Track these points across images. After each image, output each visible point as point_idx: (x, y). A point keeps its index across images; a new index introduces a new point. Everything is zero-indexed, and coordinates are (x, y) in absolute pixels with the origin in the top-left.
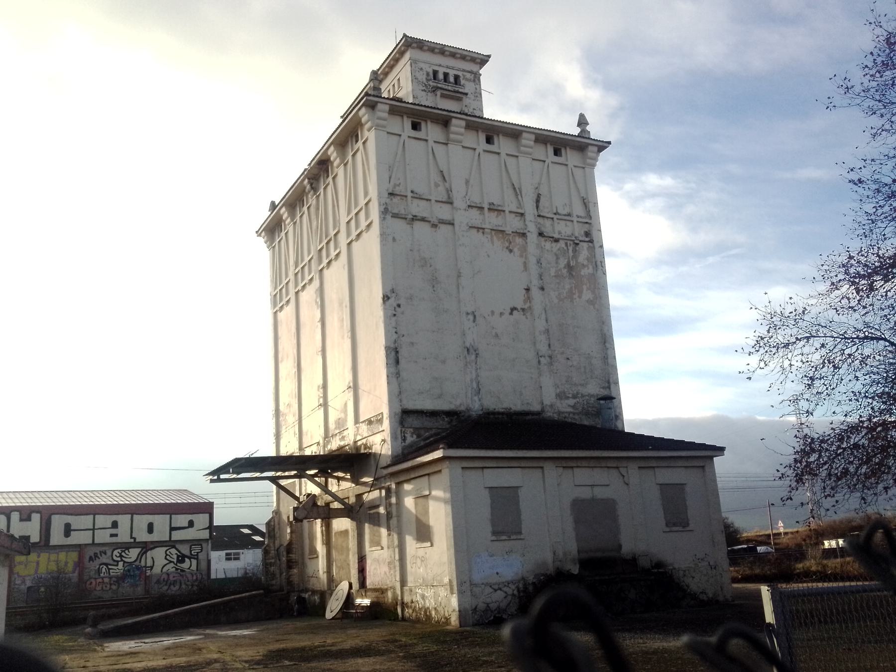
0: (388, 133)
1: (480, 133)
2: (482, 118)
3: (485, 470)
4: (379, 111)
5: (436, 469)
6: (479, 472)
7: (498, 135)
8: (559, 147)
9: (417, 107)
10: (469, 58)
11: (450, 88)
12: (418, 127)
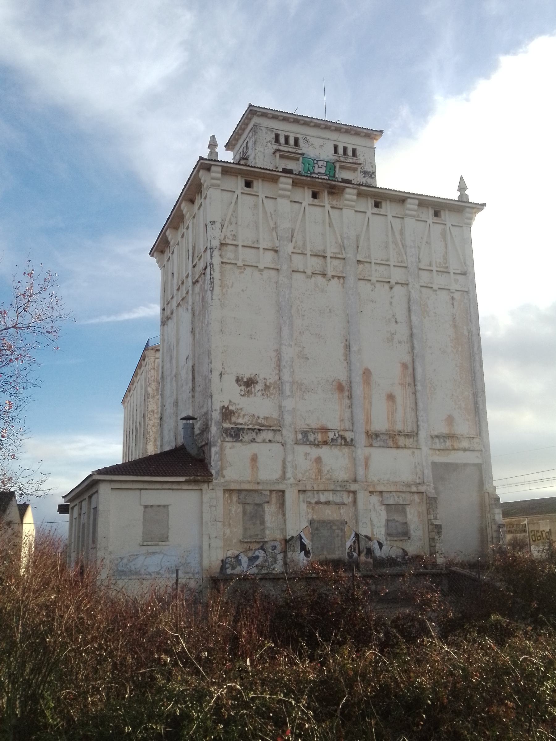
0: (221, 190)
1: (369, 199)
2: (375, 187)
3: (142, 491)
4: (212, 172)
5: (94, 490)
6: (138, 492)
7: (445, 210)
8: (251, 179)
9: (263, 171)
10: (292, 120)
11: (290, 150)
12: (380, 206)
